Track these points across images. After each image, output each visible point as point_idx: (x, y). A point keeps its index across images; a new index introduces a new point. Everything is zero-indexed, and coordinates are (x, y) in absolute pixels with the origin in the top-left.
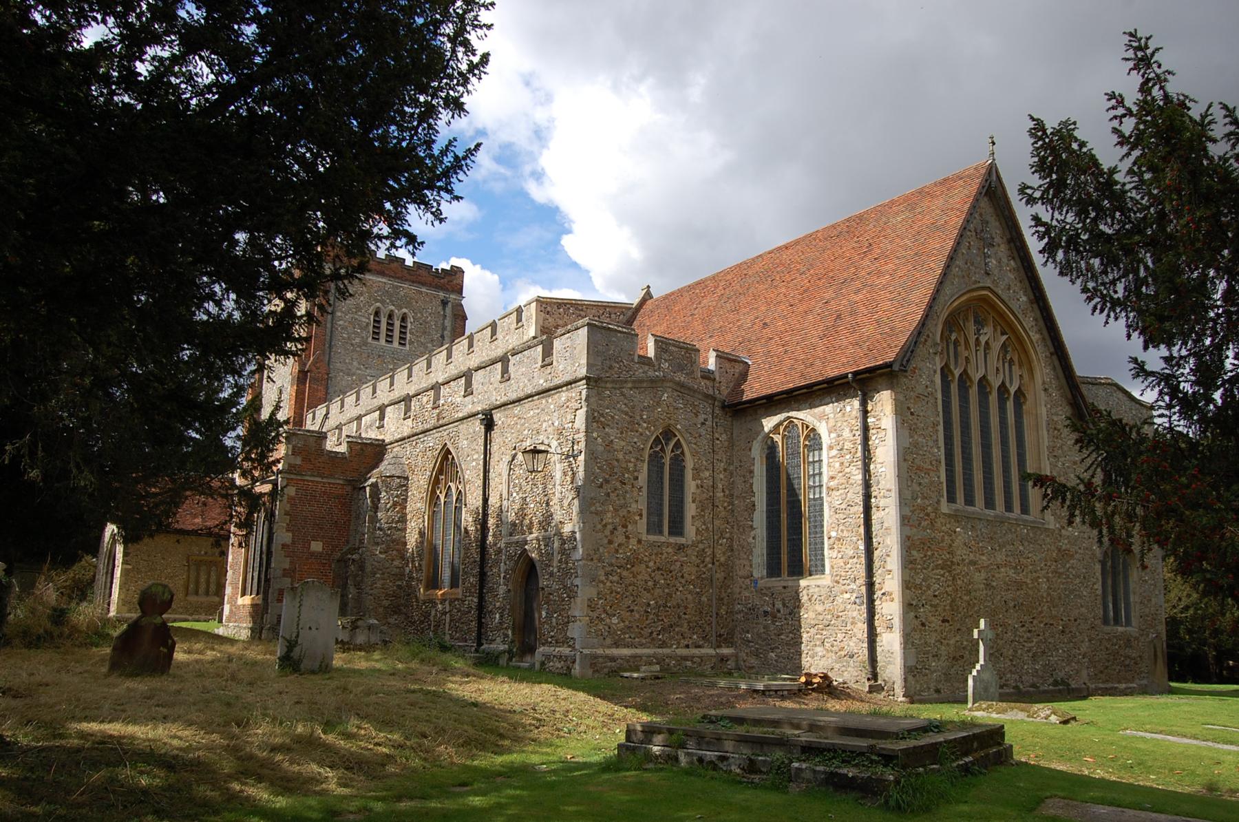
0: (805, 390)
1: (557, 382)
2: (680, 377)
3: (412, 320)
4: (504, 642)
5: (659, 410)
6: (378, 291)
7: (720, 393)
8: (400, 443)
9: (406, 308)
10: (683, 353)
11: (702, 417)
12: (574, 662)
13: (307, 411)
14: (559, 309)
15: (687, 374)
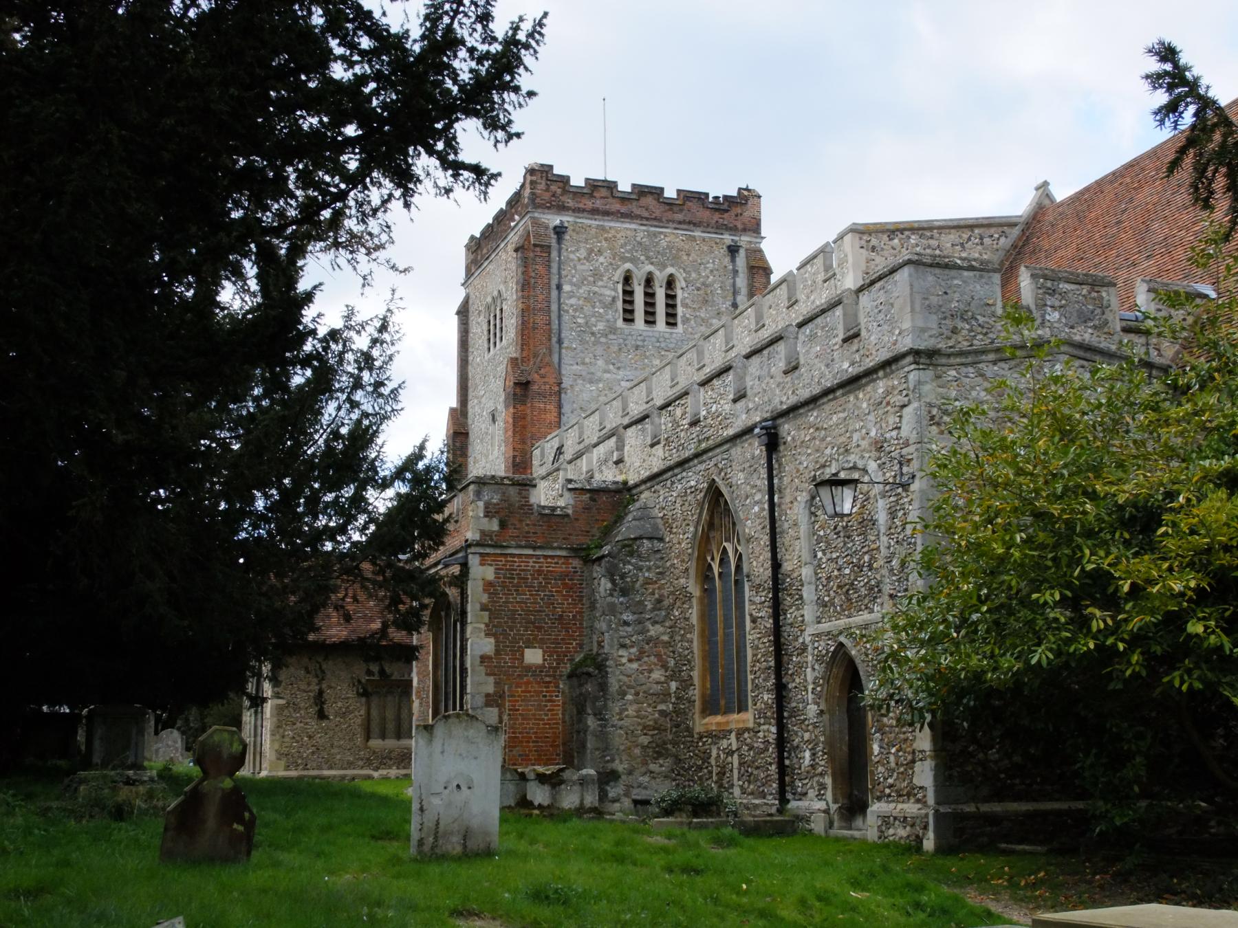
1: (869, 363)
2: (1085, 335)
3: (684, 284)
4: (820, 797)
7: (1160, 355)
8: (648, 485)
9: (672, 266)
10: (1084, 292)
12: (925, 828)
15: (1095, 327)
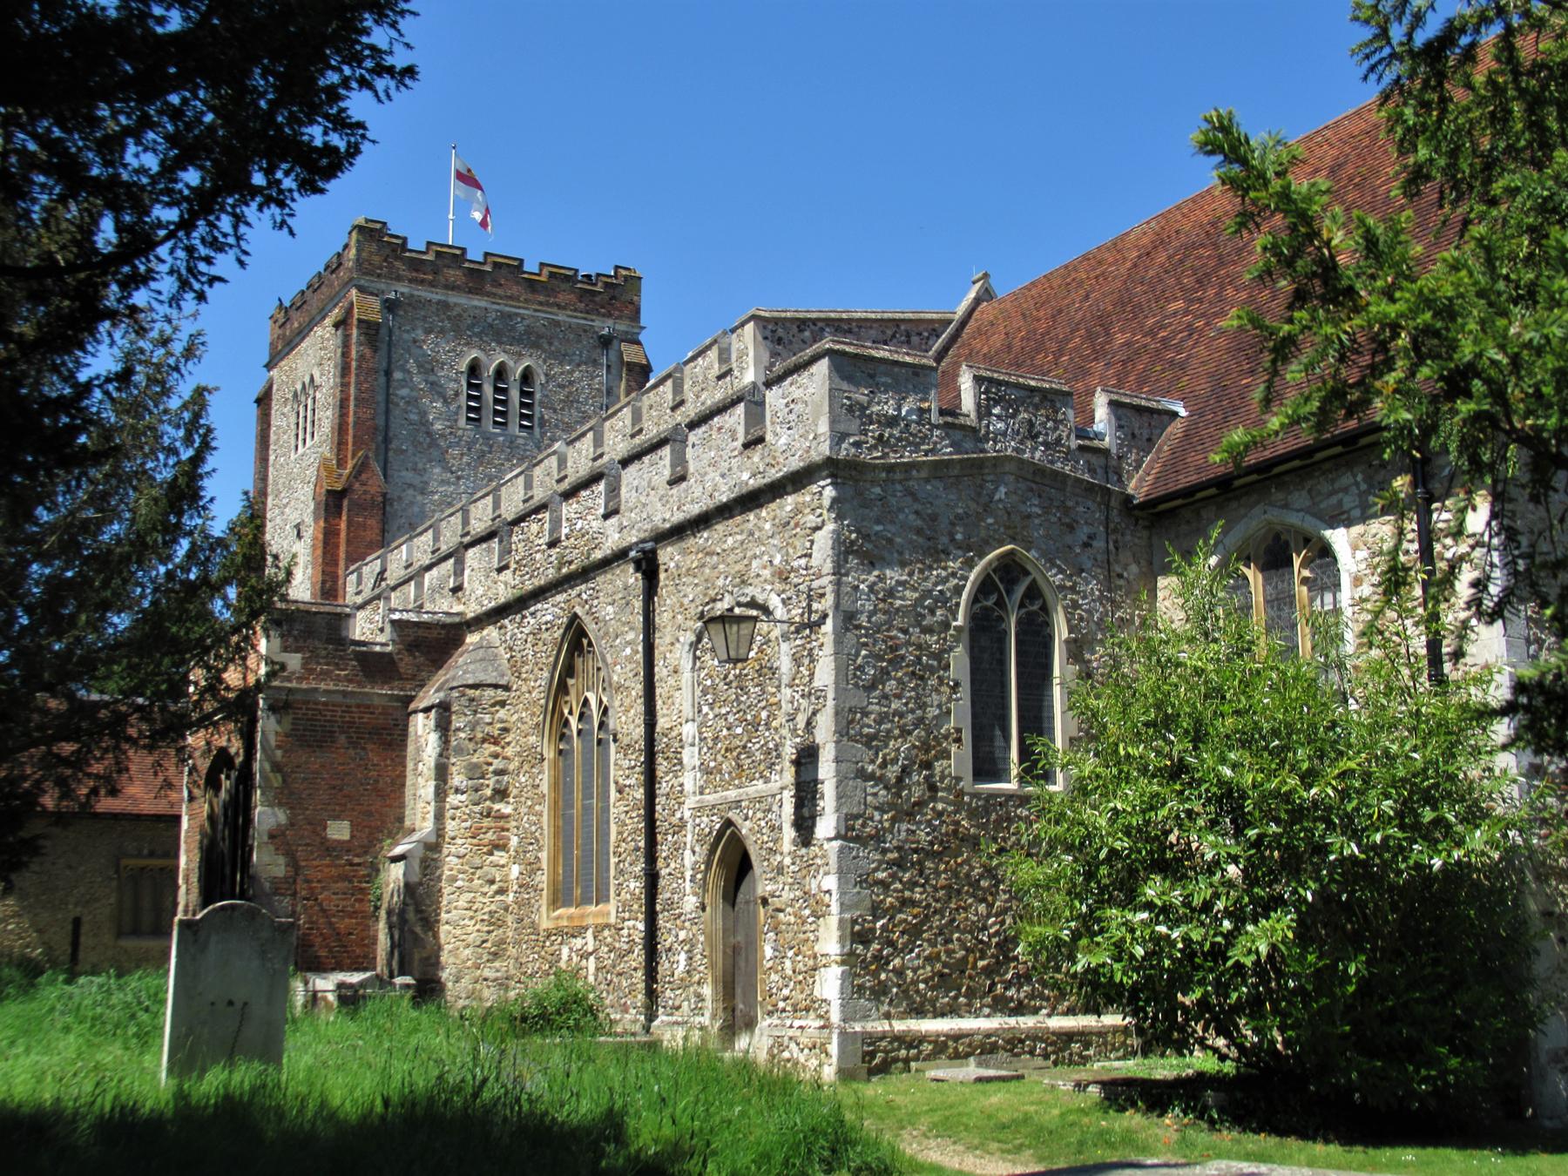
0: (1296, 463)
5: (990, 521)
11: (1083, 533)
14: (801, 331)
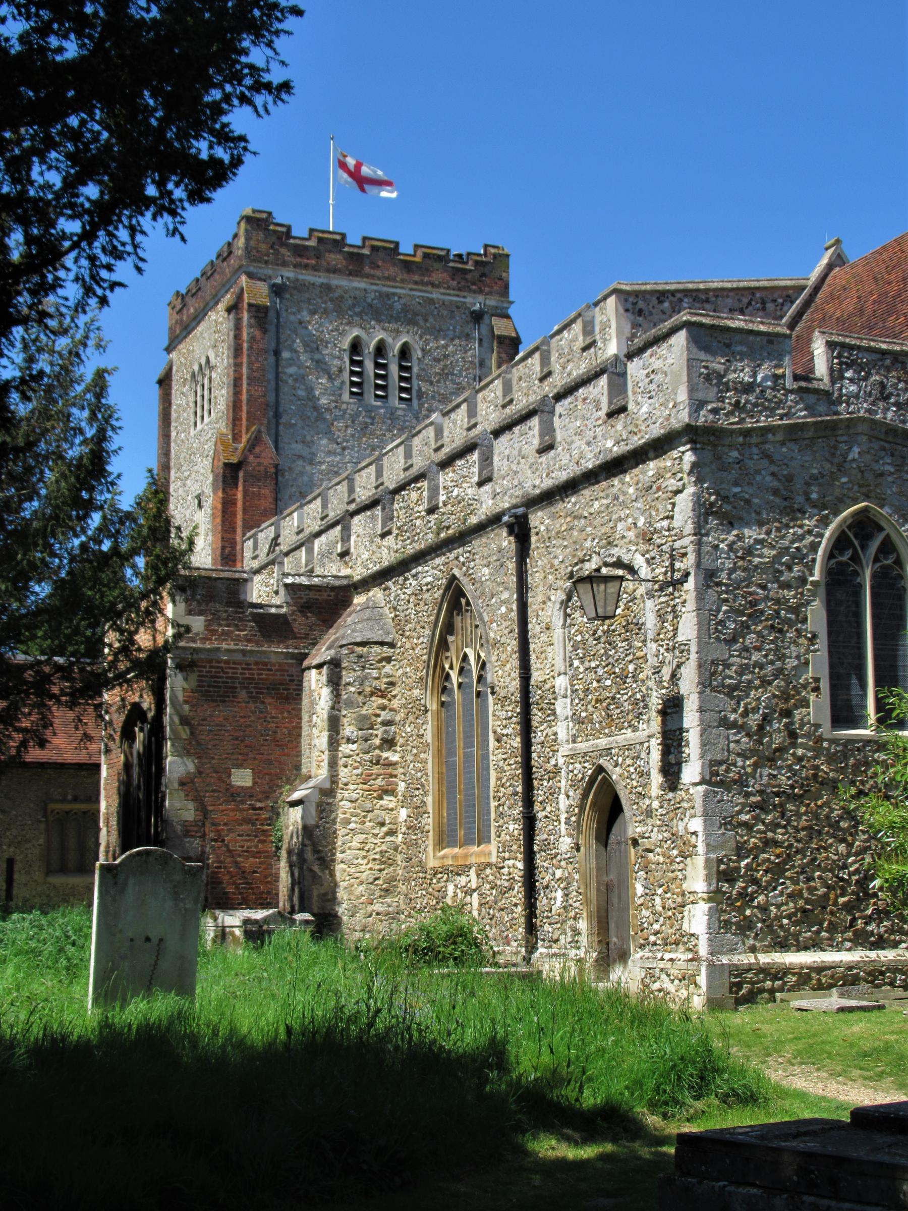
5: (844, 480)
6: (354, 306)
13: (244, 534)
